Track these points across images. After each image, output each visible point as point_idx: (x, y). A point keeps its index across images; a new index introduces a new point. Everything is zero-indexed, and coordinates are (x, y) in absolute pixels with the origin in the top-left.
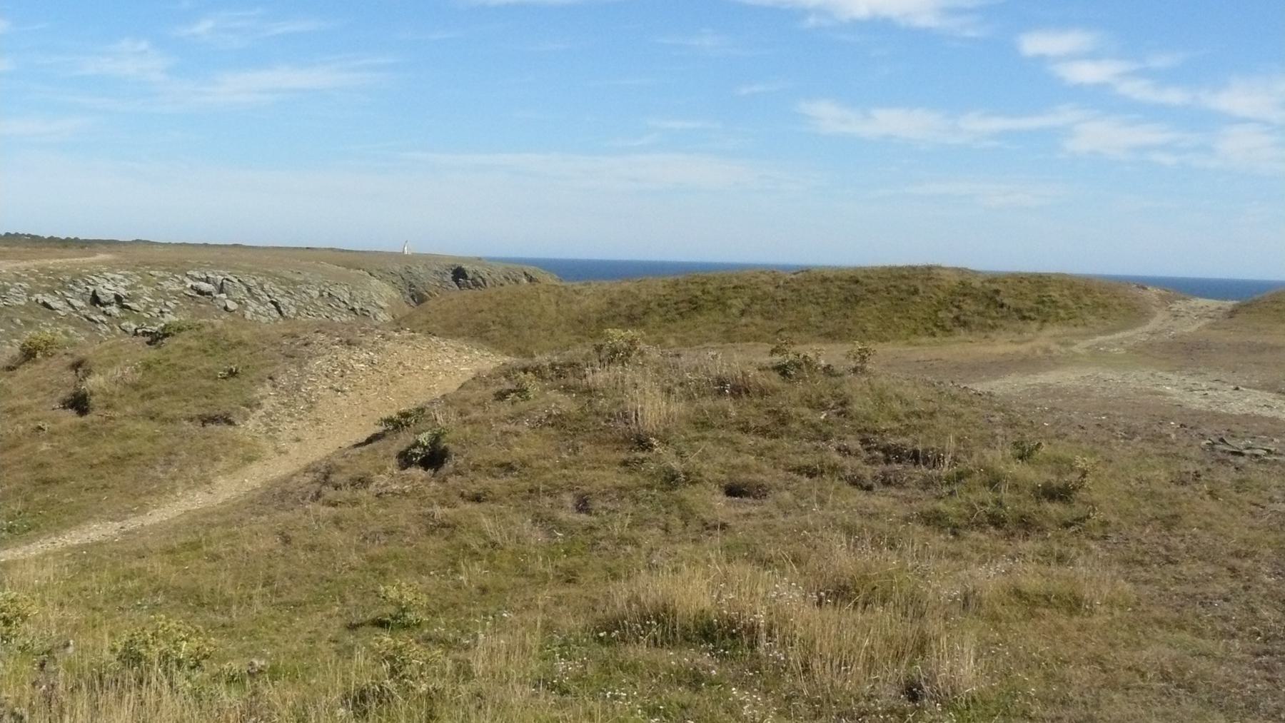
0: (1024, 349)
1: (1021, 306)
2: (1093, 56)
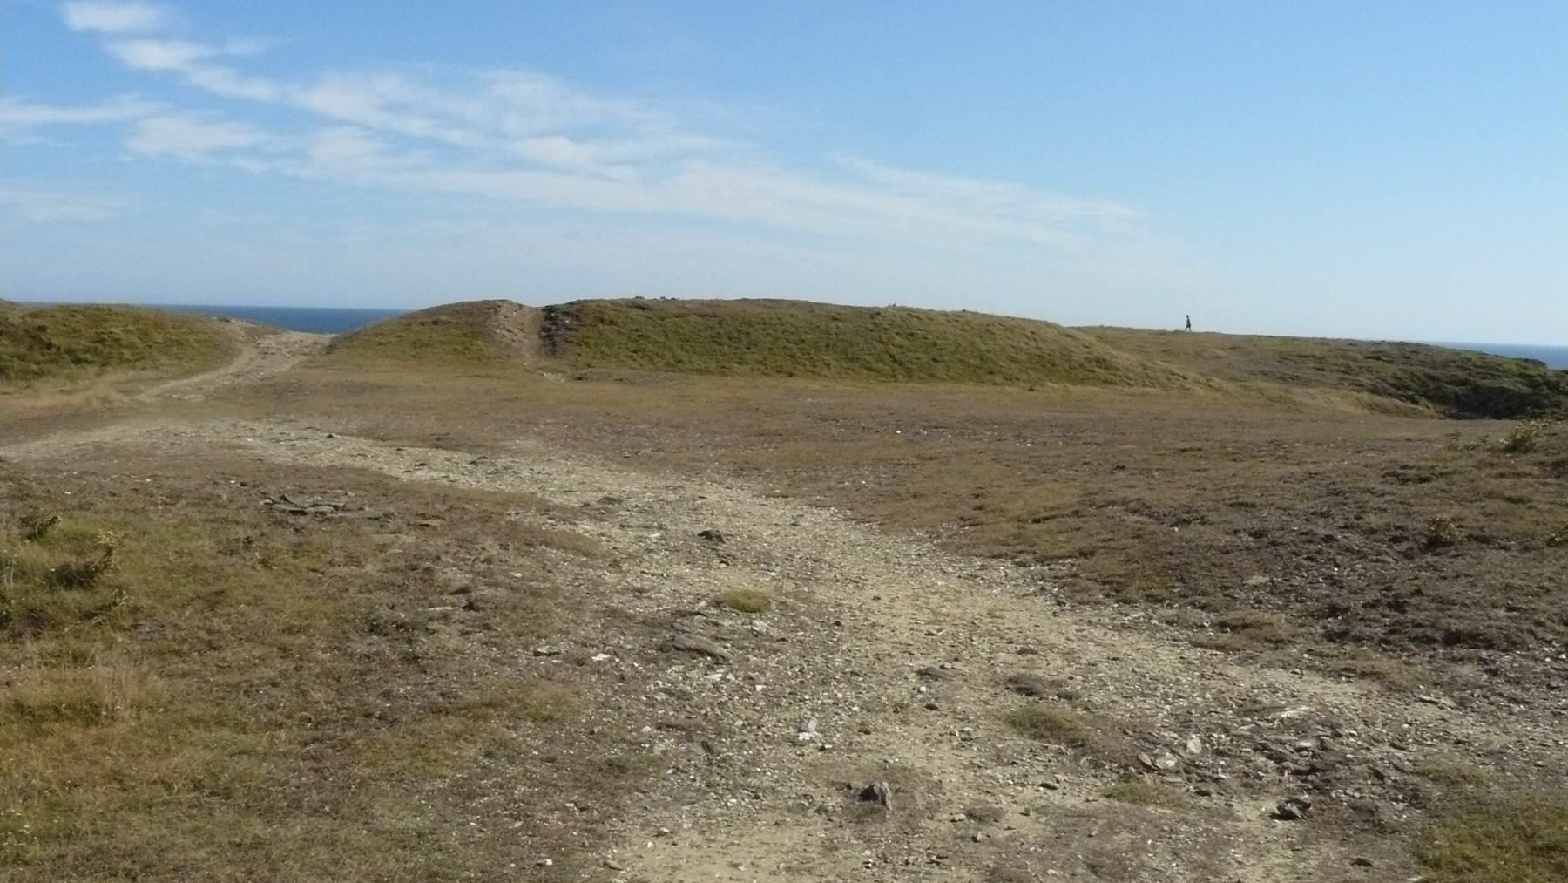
0: (77, 399)
1: (74, 346)
2: (160, 36)
